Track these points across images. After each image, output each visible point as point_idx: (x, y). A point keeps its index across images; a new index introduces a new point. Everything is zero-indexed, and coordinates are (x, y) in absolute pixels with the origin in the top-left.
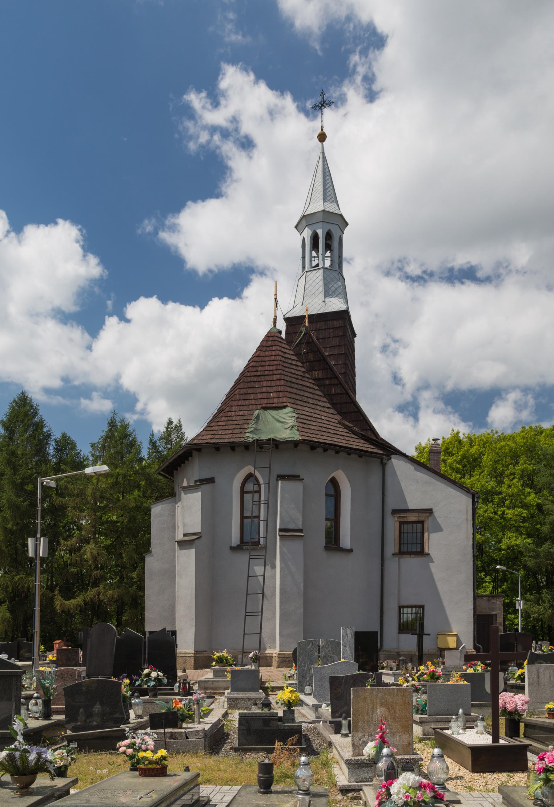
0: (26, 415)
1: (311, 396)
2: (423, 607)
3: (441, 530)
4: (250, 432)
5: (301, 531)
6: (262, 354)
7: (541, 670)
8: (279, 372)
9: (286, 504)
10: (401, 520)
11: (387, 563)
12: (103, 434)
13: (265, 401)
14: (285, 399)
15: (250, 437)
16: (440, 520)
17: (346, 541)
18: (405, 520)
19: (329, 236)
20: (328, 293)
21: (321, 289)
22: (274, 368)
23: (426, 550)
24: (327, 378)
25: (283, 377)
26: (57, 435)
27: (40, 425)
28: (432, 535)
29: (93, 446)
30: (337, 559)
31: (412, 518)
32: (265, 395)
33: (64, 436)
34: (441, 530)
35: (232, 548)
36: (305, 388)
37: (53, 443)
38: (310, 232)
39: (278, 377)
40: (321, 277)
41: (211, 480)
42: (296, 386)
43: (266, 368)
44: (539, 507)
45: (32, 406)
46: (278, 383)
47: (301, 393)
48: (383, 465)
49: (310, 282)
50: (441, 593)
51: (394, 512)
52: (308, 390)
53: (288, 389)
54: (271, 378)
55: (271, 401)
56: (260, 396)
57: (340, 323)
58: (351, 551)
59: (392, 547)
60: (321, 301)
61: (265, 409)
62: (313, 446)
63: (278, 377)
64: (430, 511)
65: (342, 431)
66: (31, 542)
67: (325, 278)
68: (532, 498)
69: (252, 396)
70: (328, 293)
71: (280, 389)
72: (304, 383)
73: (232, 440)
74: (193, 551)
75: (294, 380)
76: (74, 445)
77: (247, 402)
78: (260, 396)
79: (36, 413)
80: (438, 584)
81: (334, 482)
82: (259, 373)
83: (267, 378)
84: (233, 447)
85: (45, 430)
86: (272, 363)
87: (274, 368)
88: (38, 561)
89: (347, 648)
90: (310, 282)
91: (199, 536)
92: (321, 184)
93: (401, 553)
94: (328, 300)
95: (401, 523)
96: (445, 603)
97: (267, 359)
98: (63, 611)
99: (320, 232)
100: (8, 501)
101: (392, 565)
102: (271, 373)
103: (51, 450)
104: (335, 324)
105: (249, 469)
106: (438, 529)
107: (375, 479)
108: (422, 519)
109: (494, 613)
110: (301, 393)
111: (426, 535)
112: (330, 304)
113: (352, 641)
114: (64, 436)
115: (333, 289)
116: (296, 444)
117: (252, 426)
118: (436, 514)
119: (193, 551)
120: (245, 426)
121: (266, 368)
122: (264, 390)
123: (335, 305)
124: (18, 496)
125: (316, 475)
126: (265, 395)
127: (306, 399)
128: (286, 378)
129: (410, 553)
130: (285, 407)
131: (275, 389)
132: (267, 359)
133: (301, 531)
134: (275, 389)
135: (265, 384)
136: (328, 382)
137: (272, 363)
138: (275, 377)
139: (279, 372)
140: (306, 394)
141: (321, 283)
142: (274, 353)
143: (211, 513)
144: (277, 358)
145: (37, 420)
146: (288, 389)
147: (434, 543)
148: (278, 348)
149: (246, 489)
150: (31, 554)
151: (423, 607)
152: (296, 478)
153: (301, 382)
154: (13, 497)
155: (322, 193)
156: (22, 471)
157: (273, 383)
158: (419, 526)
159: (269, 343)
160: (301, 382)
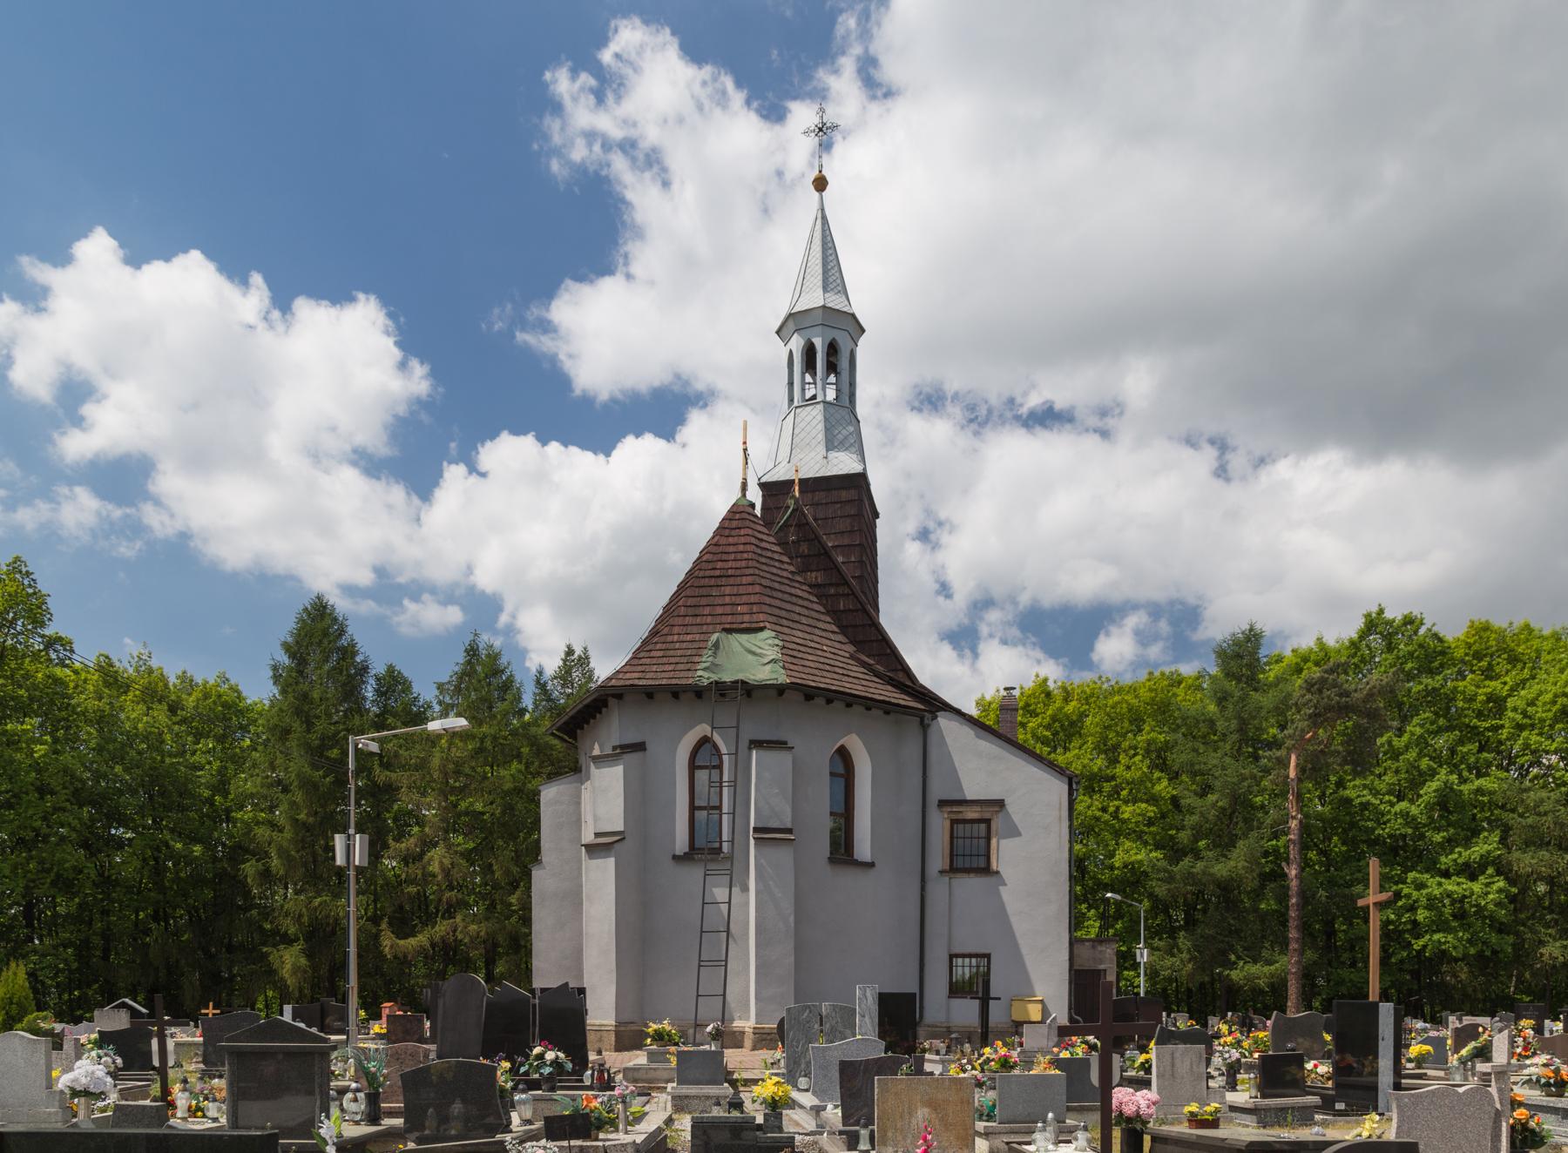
0: (325, 634)
1: (806, 612)
2: (988, 956)
3: (1019, 834)
4: (704, 669)
5: (789, 831)
6: (723, 541)
7: (1177, 1055)
8: (751, 571)
9: (764, 787)
10: (954, 817)
11: (930, 886)
12: (457, 669)
13: (729, 619)
14: (762, 616)
15: (704, 677)
16: (1016, 818)
17: (863, 847)
18: (960, 817)
19: (832, 349)
20: (831, 444)
21: (821, 436)
22: (743, 564)
23: (994, 866)
24: (831, 585)
25: (758, 580)
26: (378, 668)
27: (349, 652)
28: (1003, 842)
29: (440, 687)
30: (848, 879)
31: (971, 813)
32: (728, 609)
33: (391, 669)
34: (1019, 834)
35: (675, 857)
36: (794, 600)
37: (372, 681)
38: (802, 342)
39: (750, 579)
40: (820, 417)
41: (640, 747)
42: (780, 595)
43: (730, 564)
44: (1175, 800)
45: (335, 620)
46: (750, 589)
47: (788, 606)
48: (925, 728)
49: (802, 425)
50: (1018, 935)
51: (943, 803)
52: (800, 602)
53: (768, 600)
54: (738, 580)
55: (739, 618)
56: (719, 610)
57: (853, 494)
58: (871, 865)
59: (938, 859)
60: (820, 457)
61: (729, 631)
62: (809, 694)
63: (750, 579)
64: (1000, 804)
65: (857, 670)
66: (339, 841)
67: (826, 420)
68: (1163, 787)
69: (707, 611)
70: (831, 444)
71: (753, 599)
72: (793, 591)
73: (674, 682)
74: (612, 860)
75: (776, 586)
76: (407, 686)
77: (698, 620)
78: (719, 610)
79: (342, 632)
80: (1014, 921)
81: (843, 754)
82: (717, 573)
83: (731, 581)
84: (676, 693)
85: (358, 659)
86: (739, 556)
87: (743, 564)
88: (352, 873)
89: (867, 1019)
90: (802, 425)
91: (621, 837)
92: (819, 261)
93: (953, 869)
94: (832, 454)
95: (953, 822)
96: (1024, 951)
97: (731, 549)
98: (395, 957)
99: (818, 343)
100: (298, 775)
101: (938, 889)
102: (738, 572)
103: (369, 693)
104: (844, 495)
105: (703, 729)
106: (1014, 832)
107: (912, 750)
108: (987, 816)
109: (1102, 967)
110: (788, 606)
111: (994, 841)
112: (835, 461)
113: (875, 1008)
114: (391, 669)
115: (840, 437)
116: (781, 690)
117: (706, 659)
118: (1011, 807)
119: (612, 860)
120: (696, 659)
121: (730, 564)
122: (727, 599)
123: (844, 463)
124: (315, 767)
125: (814, 742)
126: (728, 609)
127: (797, 618)
128: (764, 582)
129: (968, 871)
130: (762, 629)
131: (744, 599)
132: (731, 549)
133: (789, 831)
134: (744, 599)
135: (728, 590)
136: (832, 591)
137: (739, 556)
138: (745, 580)
139: (751, 571)
140: (798, 609)
141: (821, 426)
142: (743, 540)
143: (639, 799)
144: (748, 548)
145: (344, 642)
146: (768, 600)
147: (1006, 854)
148: (750, 532)
149: (698, 763)
150: (340, 860)
151: (988, 956)
152: (780, 745)
153: (788, 589)
154: (307, 769)
155: (820, 277)
156: (320, 726)
157: (742, 590)
158: (983, 826)
159: (734, 524)
160: (788, 589)
